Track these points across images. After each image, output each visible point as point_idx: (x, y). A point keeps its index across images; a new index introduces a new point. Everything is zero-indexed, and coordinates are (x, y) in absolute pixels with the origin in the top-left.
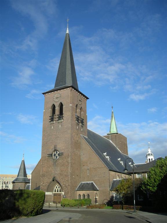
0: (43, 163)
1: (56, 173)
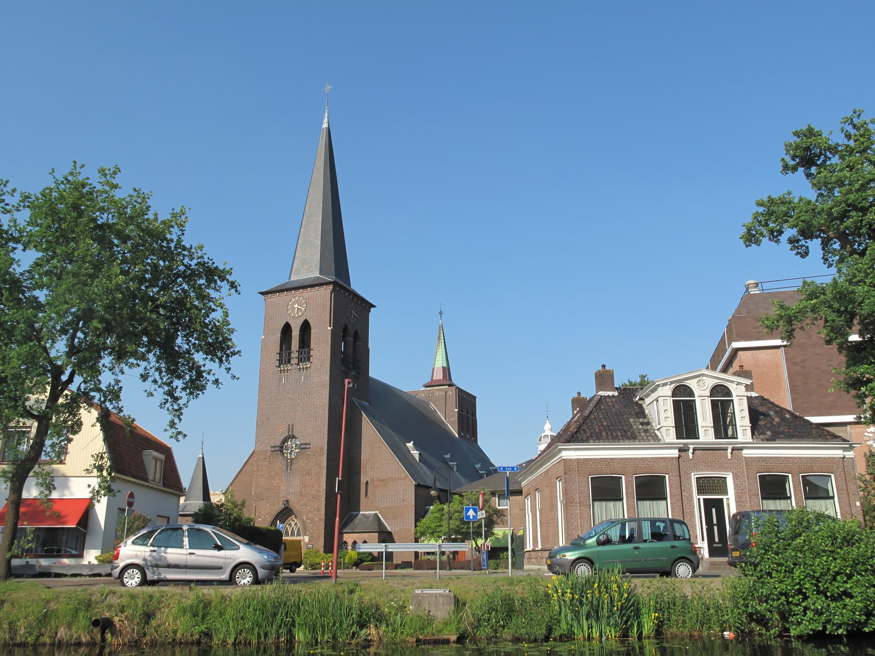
0: (260, 468)
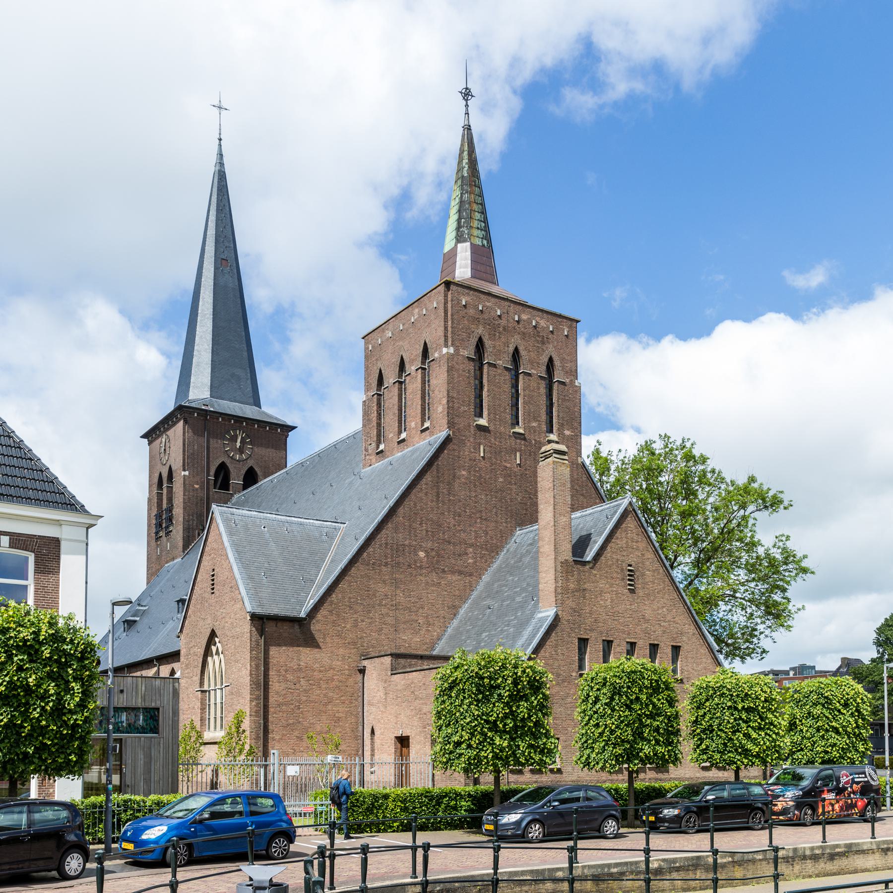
1: (648, 563)
